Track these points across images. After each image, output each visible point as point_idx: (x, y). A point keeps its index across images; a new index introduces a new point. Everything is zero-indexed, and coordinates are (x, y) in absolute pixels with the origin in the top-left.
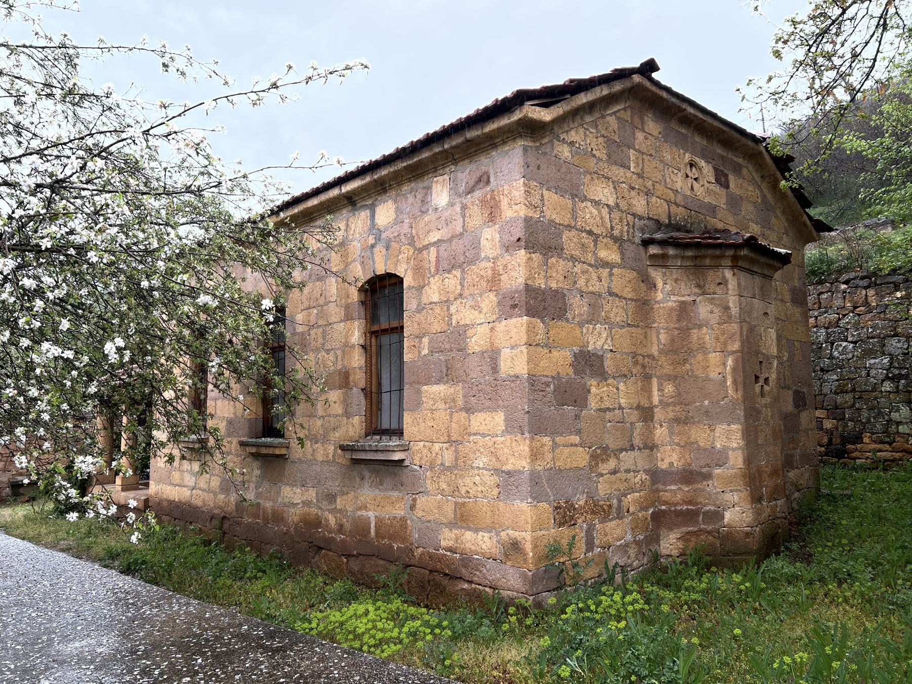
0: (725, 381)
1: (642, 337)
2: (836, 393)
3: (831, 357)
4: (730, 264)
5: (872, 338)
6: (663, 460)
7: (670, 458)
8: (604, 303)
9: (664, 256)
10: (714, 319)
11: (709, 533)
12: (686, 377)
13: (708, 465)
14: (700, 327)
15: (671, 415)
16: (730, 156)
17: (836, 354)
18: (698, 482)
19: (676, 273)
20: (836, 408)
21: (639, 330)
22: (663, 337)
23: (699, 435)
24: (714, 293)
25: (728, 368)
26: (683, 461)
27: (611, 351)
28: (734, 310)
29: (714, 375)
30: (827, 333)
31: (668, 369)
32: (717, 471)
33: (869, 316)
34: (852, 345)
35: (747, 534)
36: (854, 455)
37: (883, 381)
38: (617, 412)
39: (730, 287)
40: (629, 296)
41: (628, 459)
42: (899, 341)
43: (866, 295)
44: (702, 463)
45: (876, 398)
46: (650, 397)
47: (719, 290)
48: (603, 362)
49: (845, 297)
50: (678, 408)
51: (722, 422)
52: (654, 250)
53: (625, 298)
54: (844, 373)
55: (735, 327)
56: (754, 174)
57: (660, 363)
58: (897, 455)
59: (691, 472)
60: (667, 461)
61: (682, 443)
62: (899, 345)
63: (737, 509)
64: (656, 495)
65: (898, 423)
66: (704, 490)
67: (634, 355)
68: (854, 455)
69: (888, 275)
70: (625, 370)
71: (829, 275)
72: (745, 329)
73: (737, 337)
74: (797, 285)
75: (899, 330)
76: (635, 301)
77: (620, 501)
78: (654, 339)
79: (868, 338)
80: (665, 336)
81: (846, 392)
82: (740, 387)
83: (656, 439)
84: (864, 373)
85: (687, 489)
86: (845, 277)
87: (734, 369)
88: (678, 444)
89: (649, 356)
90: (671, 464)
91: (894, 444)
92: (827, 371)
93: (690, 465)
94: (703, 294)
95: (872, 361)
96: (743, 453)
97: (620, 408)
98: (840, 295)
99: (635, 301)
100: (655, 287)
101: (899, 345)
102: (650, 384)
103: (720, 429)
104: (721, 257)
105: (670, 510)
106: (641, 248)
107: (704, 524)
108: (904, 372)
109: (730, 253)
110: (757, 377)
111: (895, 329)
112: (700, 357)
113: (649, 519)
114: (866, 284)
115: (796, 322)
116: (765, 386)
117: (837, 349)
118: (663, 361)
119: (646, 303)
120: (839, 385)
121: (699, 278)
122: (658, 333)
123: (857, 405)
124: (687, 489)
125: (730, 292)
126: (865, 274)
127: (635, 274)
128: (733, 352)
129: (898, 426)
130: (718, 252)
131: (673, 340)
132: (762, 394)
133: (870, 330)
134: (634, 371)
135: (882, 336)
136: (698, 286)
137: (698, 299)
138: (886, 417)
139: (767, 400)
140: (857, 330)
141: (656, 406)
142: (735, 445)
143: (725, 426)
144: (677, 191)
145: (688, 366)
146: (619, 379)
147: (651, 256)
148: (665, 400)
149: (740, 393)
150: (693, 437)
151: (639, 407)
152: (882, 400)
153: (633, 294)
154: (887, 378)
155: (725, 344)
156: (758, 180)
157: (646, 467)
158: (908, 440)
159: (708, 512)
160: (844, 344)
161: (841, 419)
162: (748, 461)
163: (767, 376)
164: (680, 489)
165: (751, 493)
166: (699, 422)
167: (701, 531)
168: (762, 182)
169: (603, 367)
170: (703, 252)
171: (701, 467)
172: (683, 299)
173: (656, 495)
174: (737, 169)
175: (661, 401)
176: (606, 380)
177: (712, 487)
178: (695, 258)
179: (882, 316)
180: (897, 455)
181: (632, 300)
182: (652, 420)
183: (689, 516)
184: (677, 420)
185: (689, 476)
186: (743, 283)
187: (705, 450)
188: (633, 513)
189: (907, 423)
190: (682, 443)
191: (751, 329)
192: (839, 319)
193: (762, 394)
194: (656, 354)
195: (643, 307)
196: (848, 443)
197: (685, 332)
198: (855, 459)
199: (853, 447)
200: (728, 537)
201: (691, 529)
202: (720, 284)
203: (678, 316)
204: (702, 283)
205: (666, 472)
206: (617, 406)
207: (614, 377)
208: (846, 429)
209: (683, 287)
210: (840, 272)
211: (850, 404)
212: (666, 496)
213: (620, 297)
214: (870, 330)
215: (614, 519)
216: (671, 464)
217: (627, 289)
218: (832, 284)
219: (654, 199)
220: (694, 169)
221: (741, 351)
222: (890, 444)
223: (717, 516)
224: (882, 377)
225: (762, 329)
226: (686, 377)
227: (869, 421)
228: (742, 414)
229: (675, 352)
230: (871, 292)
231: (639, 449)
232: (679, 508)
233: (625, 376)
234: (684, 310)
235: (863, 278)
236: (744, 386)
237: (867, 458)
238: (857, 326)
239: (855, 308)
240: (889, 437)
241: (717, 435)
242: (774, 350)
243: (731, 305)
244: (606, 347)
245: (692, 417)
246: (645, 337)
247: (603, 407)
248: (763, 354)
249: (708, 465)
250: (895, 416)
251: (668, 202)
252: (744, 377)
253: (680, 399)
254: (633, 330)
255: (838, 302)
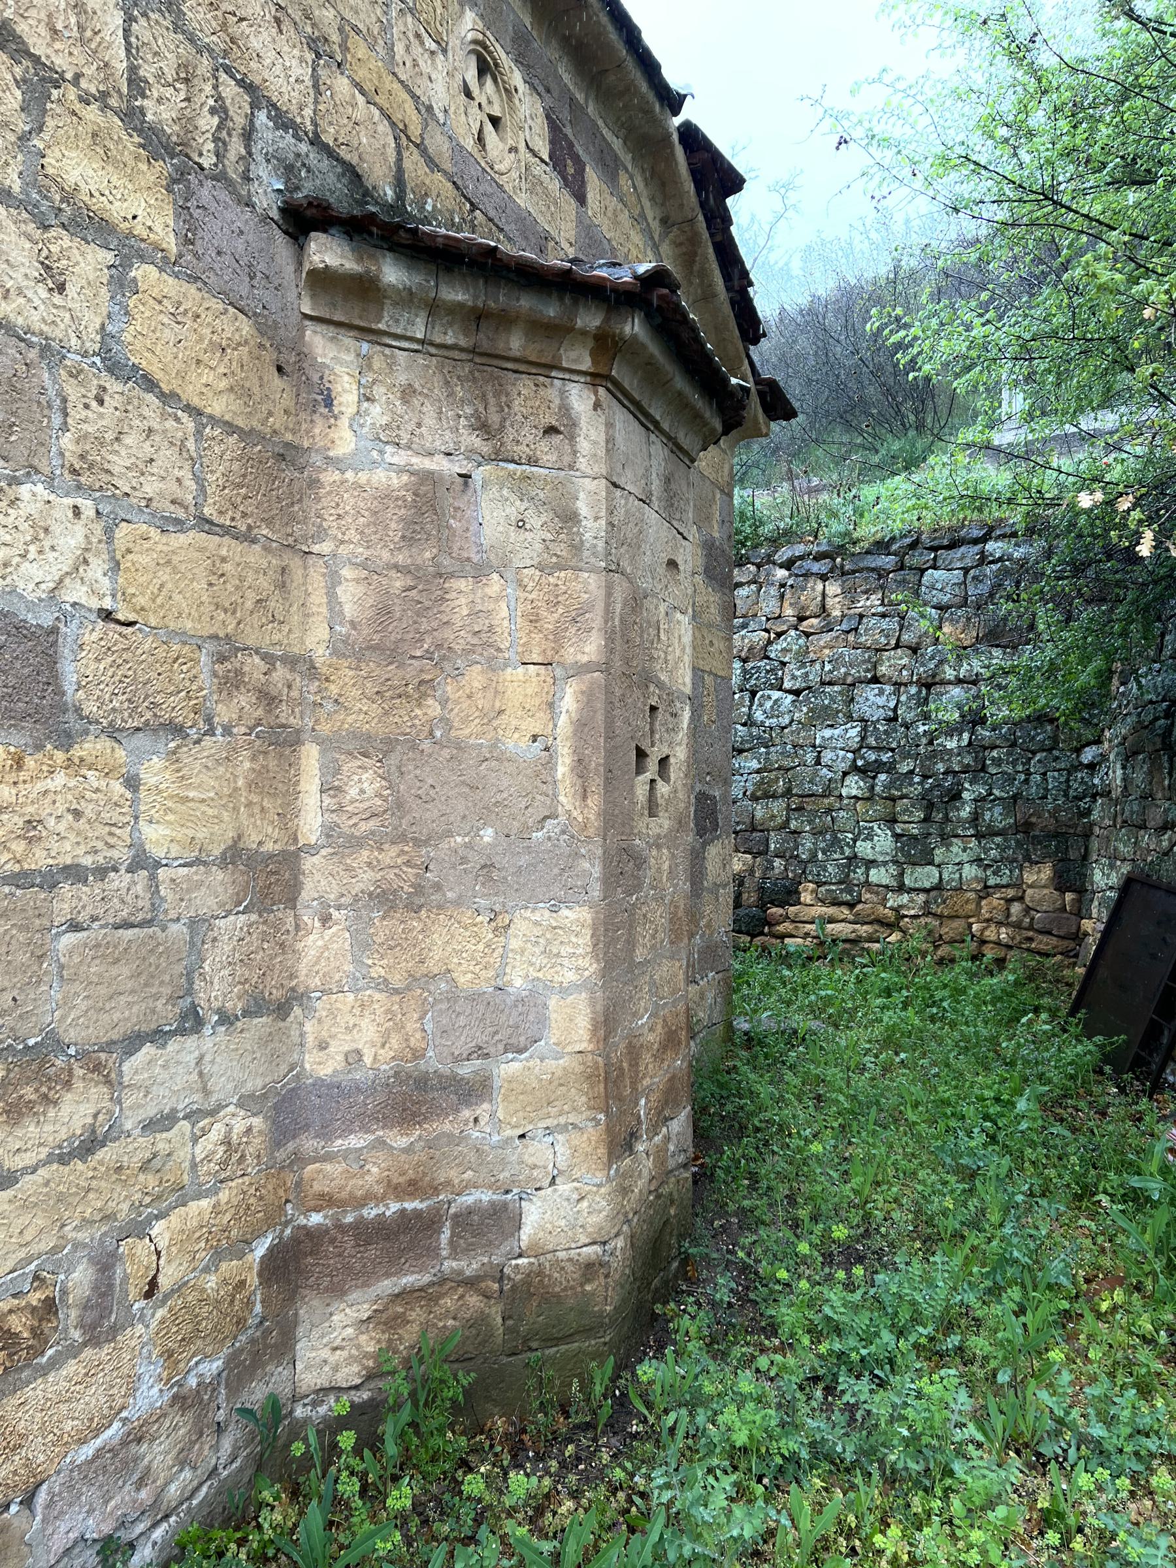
0: (550, 764)
1: (264, 582)
2: (755, 798)
3: (749, 723)
4: (586, 364)
5: (830, 683)
6: (323, 1046)
7: (348, 1037)
8: (73, 391)
9: (364, 289)
10: (528, 547)
11: (471, 1283)
12: (426, 745)
13: (479, 1051)
14: (480, 572)
15: (366, 879)
16: (591, 109)
17: (759, 716)
18: (442, 1113)
19: (406, 368)
20: (753, 829)
21: (254, 555)
22: (352, 596)
23: (457, 947)
24: (532, 461)
25: (563, 720)
26: (395, 1042)
27: (107, 616)
28: (592, 529)
29: (516, 743)
30: (745, 671)
31: (363, 714)
32: (508, 1069)
33: (827, 637)
34: (790, 697)
35: (590, 1269)
36: (781, 928)
37: (845, 774)
38: (119, 881)
39: (584, 445)
40: (217, 407)
41: (161, 1075)
42: (881, 693)
43: (824, 595)
44: (461, 1045)
45: (829, 811)
46: (287, 815)
47: (547, 451)
48: (52, 661)
49: (782, 596)
50: (390, 854)
51: (532, 901)
52: (327, 252)
53: (194, 412)
54: (773, 757)
55: (589, 585)
56: (647, 204)
57: (334, 689)
58: (864, 930)
59: (422, 1082)
60: (338, 1049)
61: (397, 981)
62: (881, 701)
63: (564, 1188)
64: (290, 1179)
65: (870, 863)
66: (462, 1138)
67: (227, 649)
68: (781, 928)
69: (868, 552)
70: (176, 708)
71: (755, 547)
72: (619, 596)
73: (596, 618)
74: (716, 535)
75: (883, 669)
76: (246, 435)
77: (105, 1263)
78: (318, 599)
79: (823, 683)
80: (361, 589)
81: (774, 796)
82: (596, 784)
83: (303, 969)
84: (810, 758)
85: (402, 1142)
86: (784, 554)
87: (581, 726)
88: (383, 984)
89: (292, 661)
90: (354, 1058)
91: (860, 907)
92: (741, 751)
93: (418, 1054)
94: (498, 457)
95: (828, 733)
96: (592, 1002)
97: (142, 862)
98: (773, 591)
99: (246, 435)
100: (329, 402)
101: (881, 701)
102: (292, 764)
103: (527, 922)
104: (558, 332)
105: (340, 1227)
106: (280, 238)
107: (454, 1255)
108: (886, 757)
109: (590, 319)
110: (641, 754)
111: (875, 668)
112: (475, 677)
113: (253, 1280)
114: (824, 570)
115: (710, 626)
116: (660, 783)
117: (761, 705)
118: (345, 680)
119: (288, 455)
120: (762, 782)
121: (484, 398)
122: (334, 580)
123: (793, 825)
124: (402, 1142)
125: (582, 463)
126: (824, 548)
127: (246, 327)
128: (582, 669)
129: (868, 869)
130: (551, 310)
131: (384, 612)
132: (652, 808)
133: (828, 667)
134: (224, 713)
135: (849, 680)
136: (482, 427)
137: (478, 475)
138: (847, 851)
139: (663, 823)
140: (803, 665)
141: (312, 850)
142: (571, 976)
143: (542, 914)
144: (429, 109)
145: (433, 708)
146: (140, 740)
147: (313, 273)
148: (346, 824)
149: (594, 802)
150: (437, 954)
151: (234, 855)
152: (842, 813)
153: (237, 405)
154: (855, 768)
155: (557, 638)
156: (655, 225)
157: (255, 1084)
158: (885, 899)
159: (470, 1211)
160: (776, 695)
161: (760, 853)
162: (607, 1023)
163: (666, 751)
164: (381, 1143)
165: (609, 1130)
166: (458, 903)
167: (443, 1281)
168: (662, 240)
169: (53, 680)
170: (501, 299)
171: (457, 1060)
172: (428, 464)
173: (290, 1179)
174: (610, 169)
175: (329, 831)
176: (66, 740)
177: (486, 1125)
178: (476, 318)
179: (851, 637)
180: (864, 930)
181: (230, 428)
182: (292, 901)
183: (405, 1237)
184: (384, 899)
185: (415, 1096)
186: (620, 438)
187: (474, 998)
188: (179, 1289)
189: (885, 863)
190: (397, 981)
191: (636, 601)
192: (769, 642)
193: (652, 808)
194: (321, 655)
195: (277, 472)
196: (772, 902)
197: (430, 583)
198: (782, 937)
199: (780, 911)
200: (534, 1307)
201: (409, 1280)
202: (551, 430)
203: (408, 523)
204: (494, 418)
205: (332, 1090)
206: (122, 854)
207: (113, 733)
208: (770, 874)
209: (429, 420)
210: (775, 542)
211: (779, 820)
212: (327, 1176)
213: (167, 398)
214: (828, 667)
215: (73, 1351)
216: (354, 1058)
217: (207, 377)
218: (759, 566)
219: (342, 85)
220: (489, 81)
221: (605, 668)
222: (851, 906)
223: (501, 1219)
224: (843, 766)
225: (662, 608)
226: (426, 745)
227: (814, 855)
228: (597, 871)
229: (392, 654)
230: (833, 588)
231: (226, 1019)
232: (370, 1212)
233: (177, 730)
234: (429, 505)
235: (819, 557)
236: (608, 782)
237: (807, 935)
238: (803, 657)
239: (801, 619)
240: (850, 892)
241: (514, 944)
242: (684, 680)
243: (583, 507)
244: (75, 593)
245: (438, 887)
246: (283, 586)
247: (39, 860)
248: (660, 685)
249: (479, 1051)
250: (864, 849)
251: (400, 131)
252: (610, 753)
253: (399, 824)
254: (227, 546)
255: (769, 606)
